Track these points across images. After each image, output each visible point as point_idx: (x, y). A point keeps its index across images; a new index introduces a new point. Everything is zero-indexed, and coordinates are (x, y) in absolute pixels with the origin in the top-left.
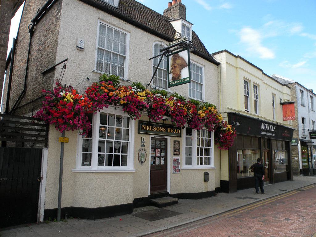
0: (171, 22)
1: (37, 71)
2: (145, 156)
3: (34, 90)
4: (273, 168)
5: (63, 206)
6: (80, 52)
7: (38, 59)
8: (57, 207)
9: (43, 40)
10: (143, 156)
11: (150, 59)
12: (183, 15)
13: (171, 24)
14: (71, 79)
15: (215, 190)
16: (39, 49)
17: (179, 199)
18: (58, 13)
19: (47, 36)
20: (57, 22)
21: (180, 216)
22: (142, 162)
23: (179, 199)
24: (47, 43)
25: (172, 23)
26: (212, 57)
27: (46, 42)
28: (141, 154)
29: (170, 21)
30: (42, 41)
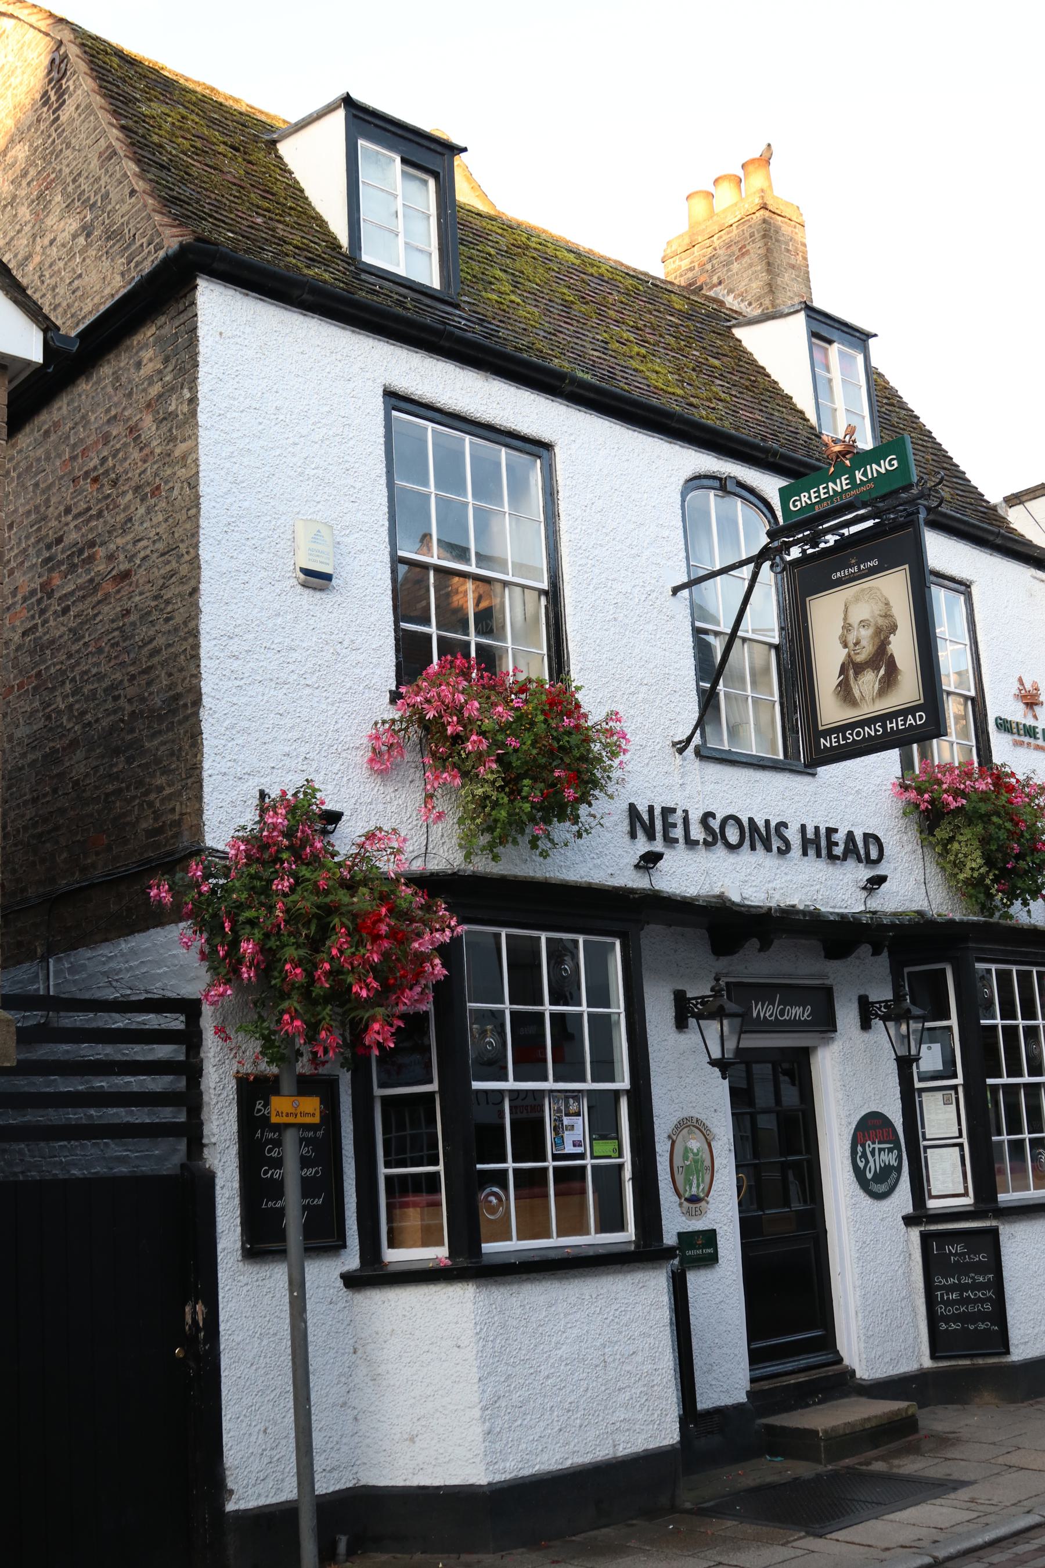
0: (738, 332)
1: (48, 718)
2: (708, 1163)
3: (41, 835)
4: (66, 1177)
5: (324, 1486)
6: (318, 595)
7: (39, 649)
8: (288, 1491)
9: (74, 536)
10: (696, 1161)
11: (676, 590)
12: (793, 267)
13: (737, 345)
14: (287, 761)
15: (743, 1398)
16: (47, 590)
17: (920, 1408)
18: (171, 389)
19: (100, 514)
20: (172, 439)
21: (964, 1494)
22: (694, 1200)
23: (920, 1408)
24: (111, 557)
25: (749, 337)
26: (1003, 520)
27: (101, 552)
28: (687, 1150)
29: (730, 327)
30: (59, 540)
